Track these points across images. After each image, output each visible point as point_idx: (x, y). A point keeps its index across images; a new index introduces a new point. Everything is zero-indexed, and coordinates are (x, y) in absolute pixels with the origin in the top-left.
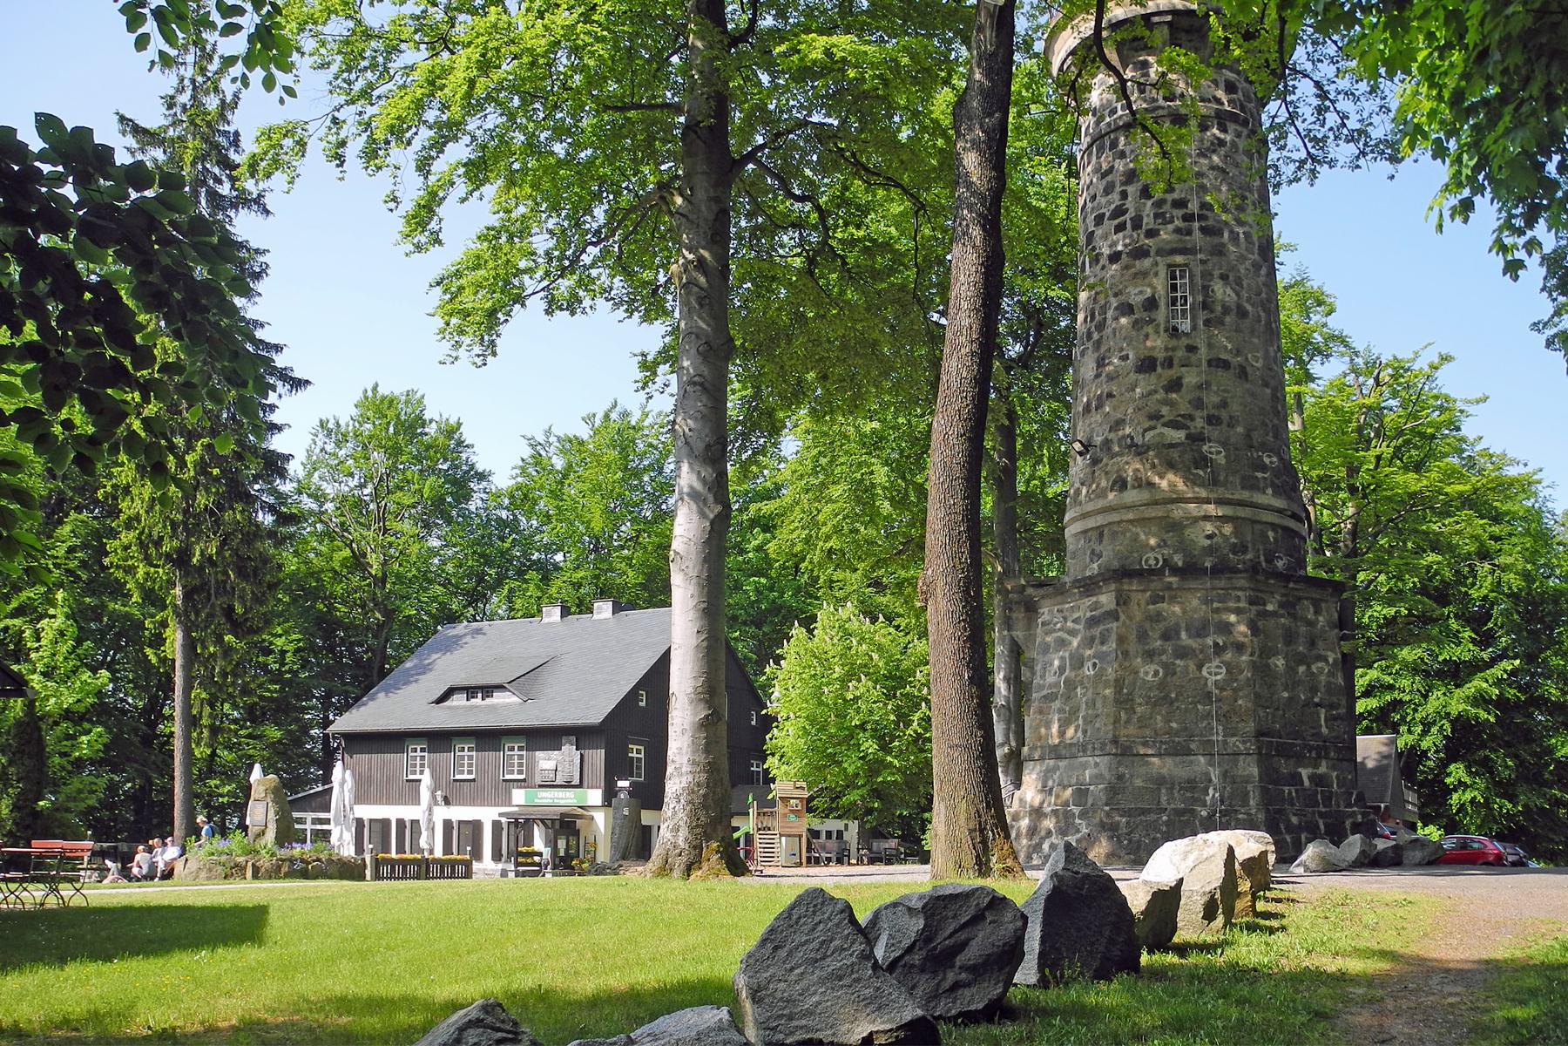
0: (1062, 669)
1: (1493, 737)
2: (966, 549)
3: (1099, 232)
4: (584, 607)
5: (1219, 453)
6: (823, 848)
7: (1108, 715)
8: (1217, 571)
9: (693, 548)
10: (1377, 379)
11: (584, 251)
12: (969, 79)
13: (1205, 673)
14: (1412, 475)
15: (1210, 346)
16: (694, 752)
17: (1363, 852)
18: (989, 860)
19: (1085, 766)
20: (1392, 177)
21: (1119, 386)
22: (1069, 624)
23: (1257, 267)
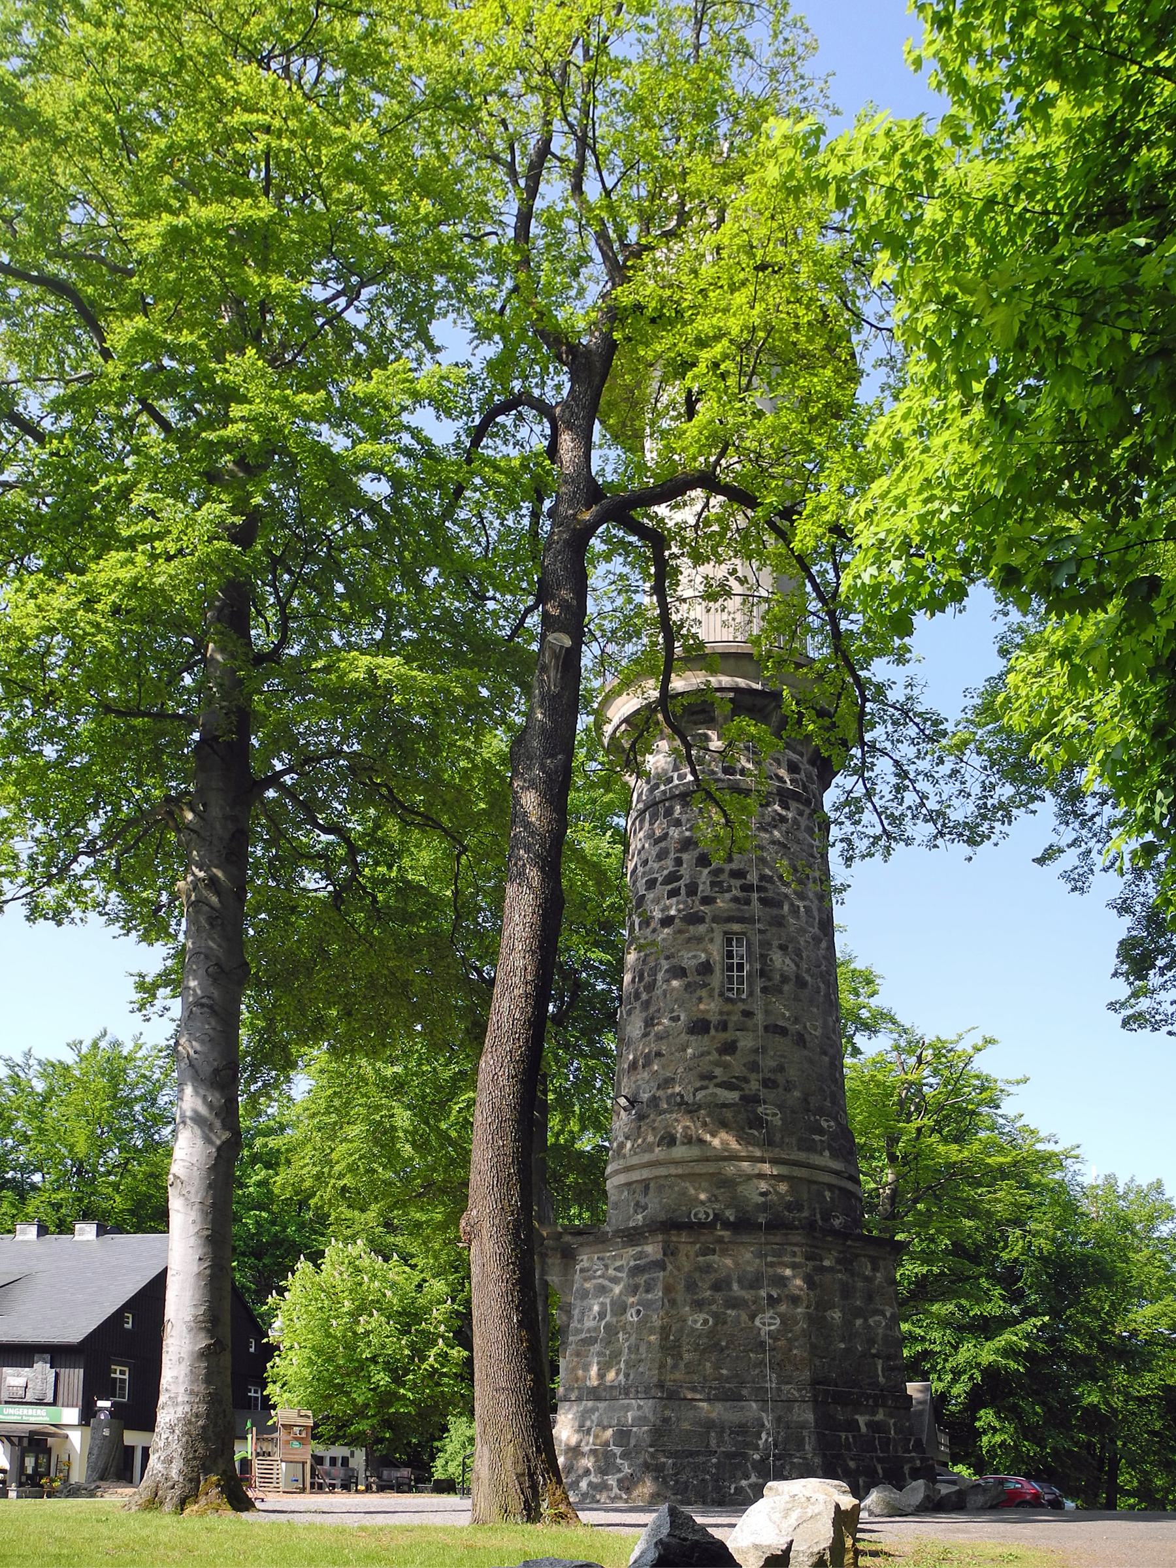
0: (602, 1315)
1: (1021, 1386)
2: (516, 1192)
3: (650, 896)
4: (64, 1228)
5: (775, 1115)
6: (328, 1474)
7: (653, 1360)
8: (775, 1225)
9: (196, 1173)
10: (919, 1058)
11: (75, 860)
12: (529, 715)
13: (757, 1322)
14: (955, 1147)
15: (767, 1012)
16: (192, 1382)
17: (927, 1497)
18: (538, 1506)
19: (627, 1408)
20: (970, 859)
21: (669, 1046)
22: (611, 1272)
23: (817, 940)
